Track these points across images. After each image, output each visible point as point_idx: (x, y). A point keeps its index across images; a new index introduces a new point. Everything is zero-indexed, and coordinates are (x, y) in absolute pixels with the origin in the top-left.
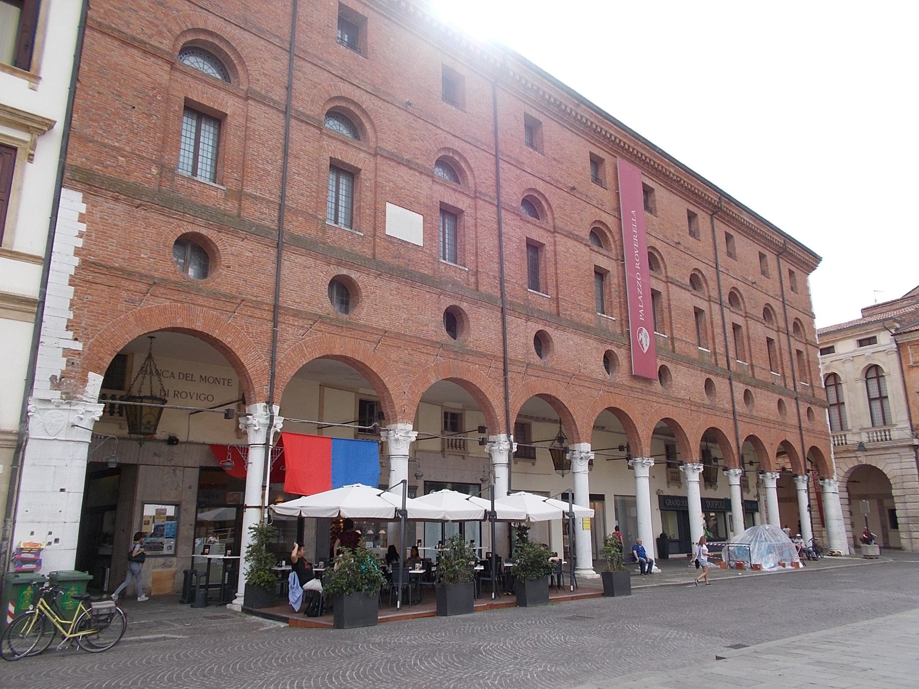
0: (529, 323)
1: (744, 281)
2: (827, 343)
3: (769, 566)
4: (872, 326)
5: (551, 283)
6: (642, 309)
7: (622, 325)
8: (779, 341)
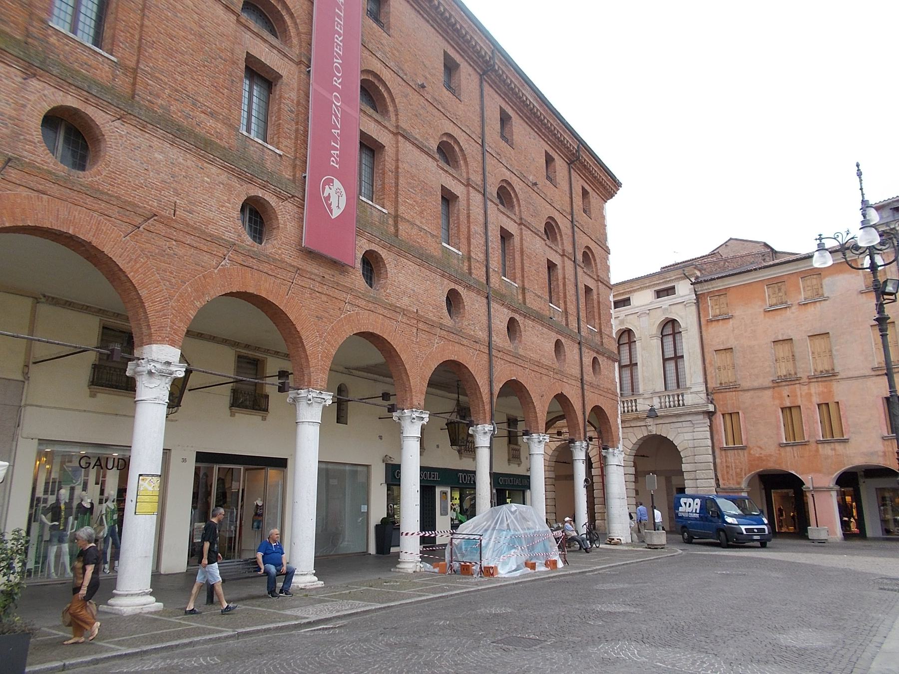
0: (34, 83)
1: (522, 178)
2: (623, 294)
3: (507, 569)
4: (671, 274)
6: (340, 151)
7: (294, 167)
8: (564, 267)
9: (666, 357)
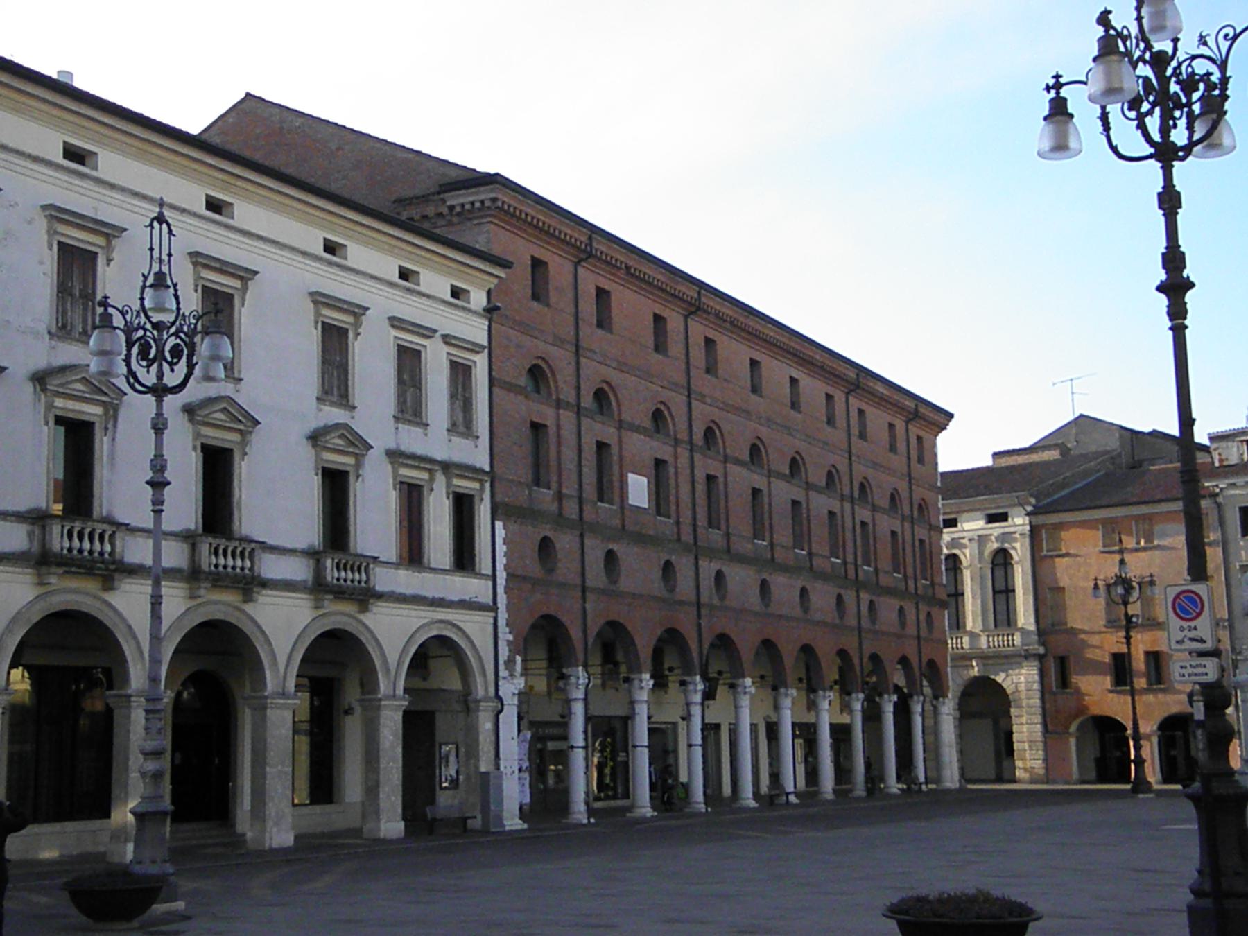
5: (554, 478)
9: (997, 589)
